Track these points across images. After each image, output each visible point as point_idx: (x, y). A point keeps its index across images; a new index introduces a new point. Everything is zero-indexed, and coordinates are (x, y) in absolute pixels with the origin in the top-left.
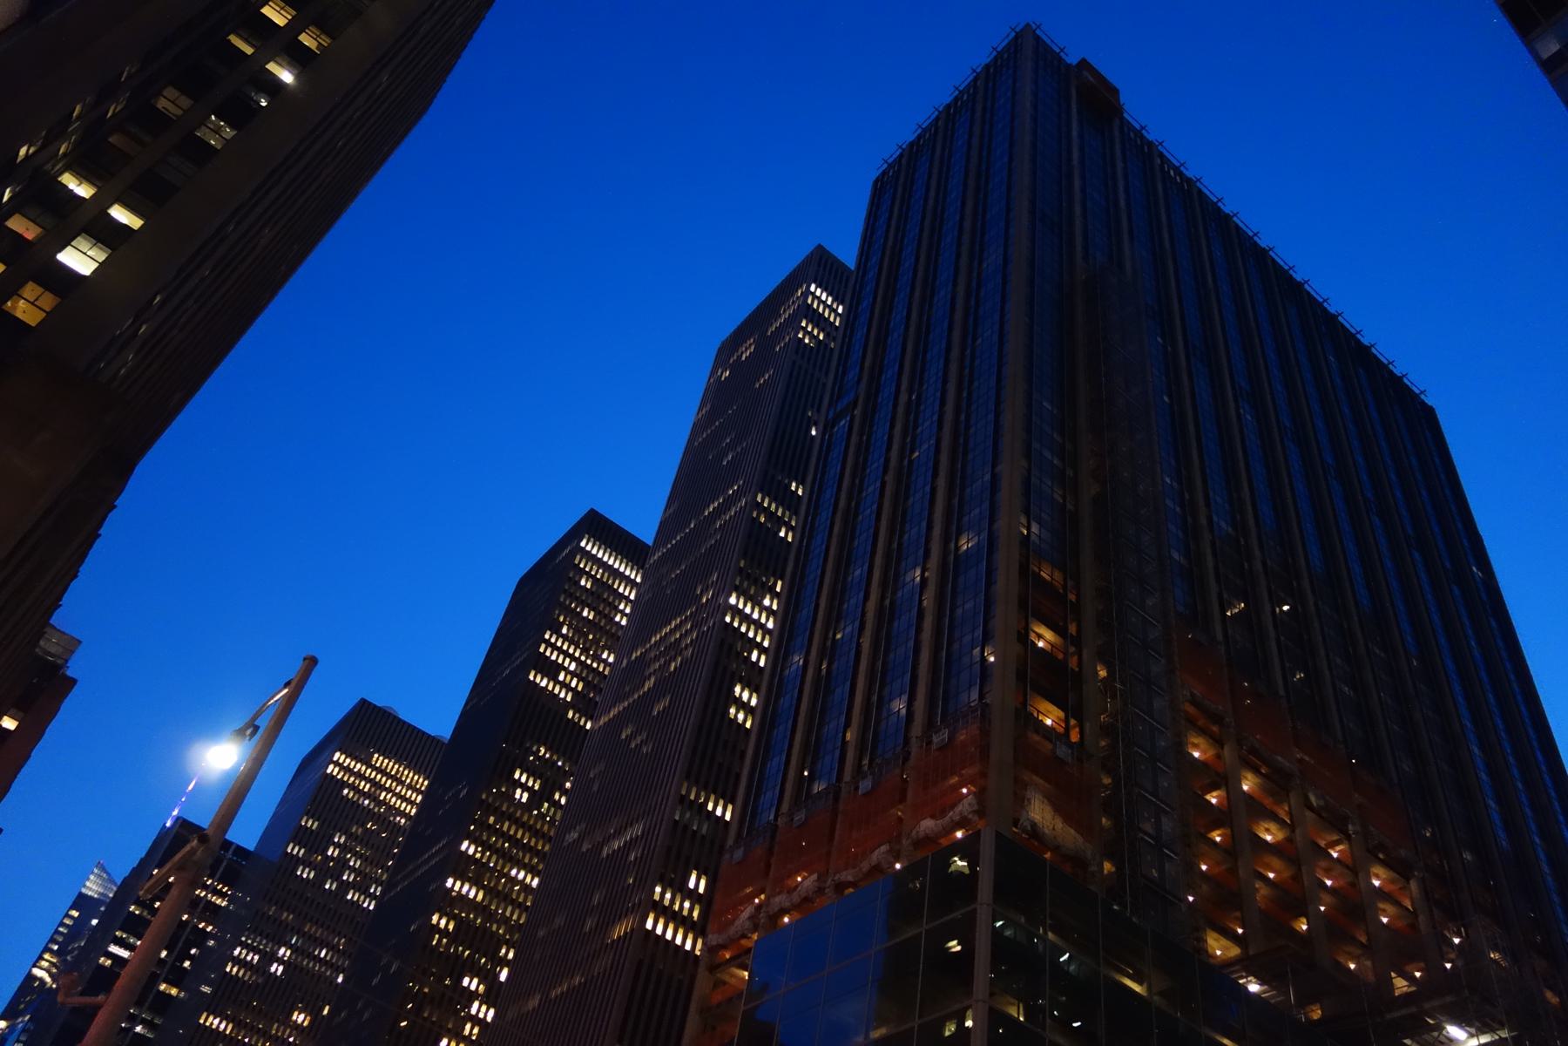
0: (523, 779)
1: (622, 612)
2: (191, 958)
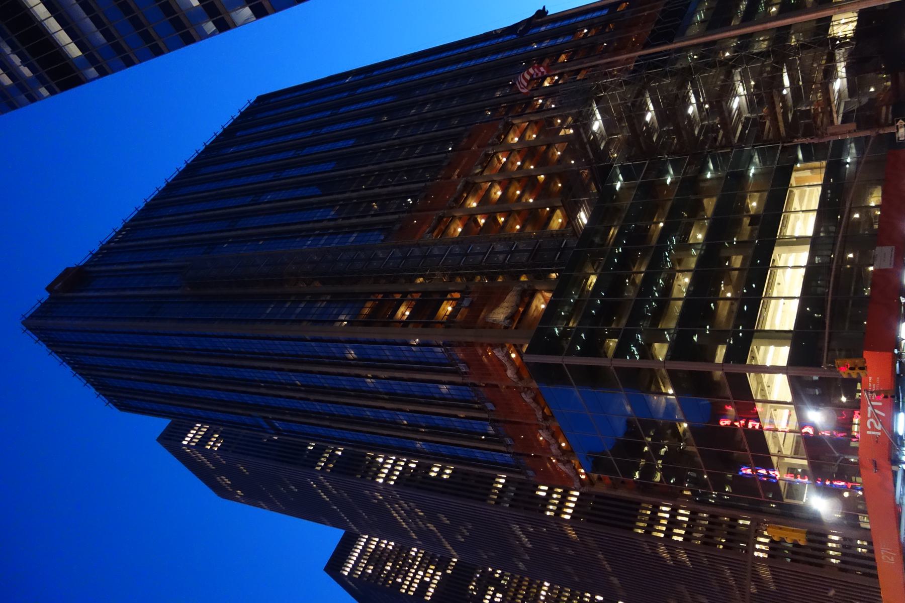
1: (386, 545)
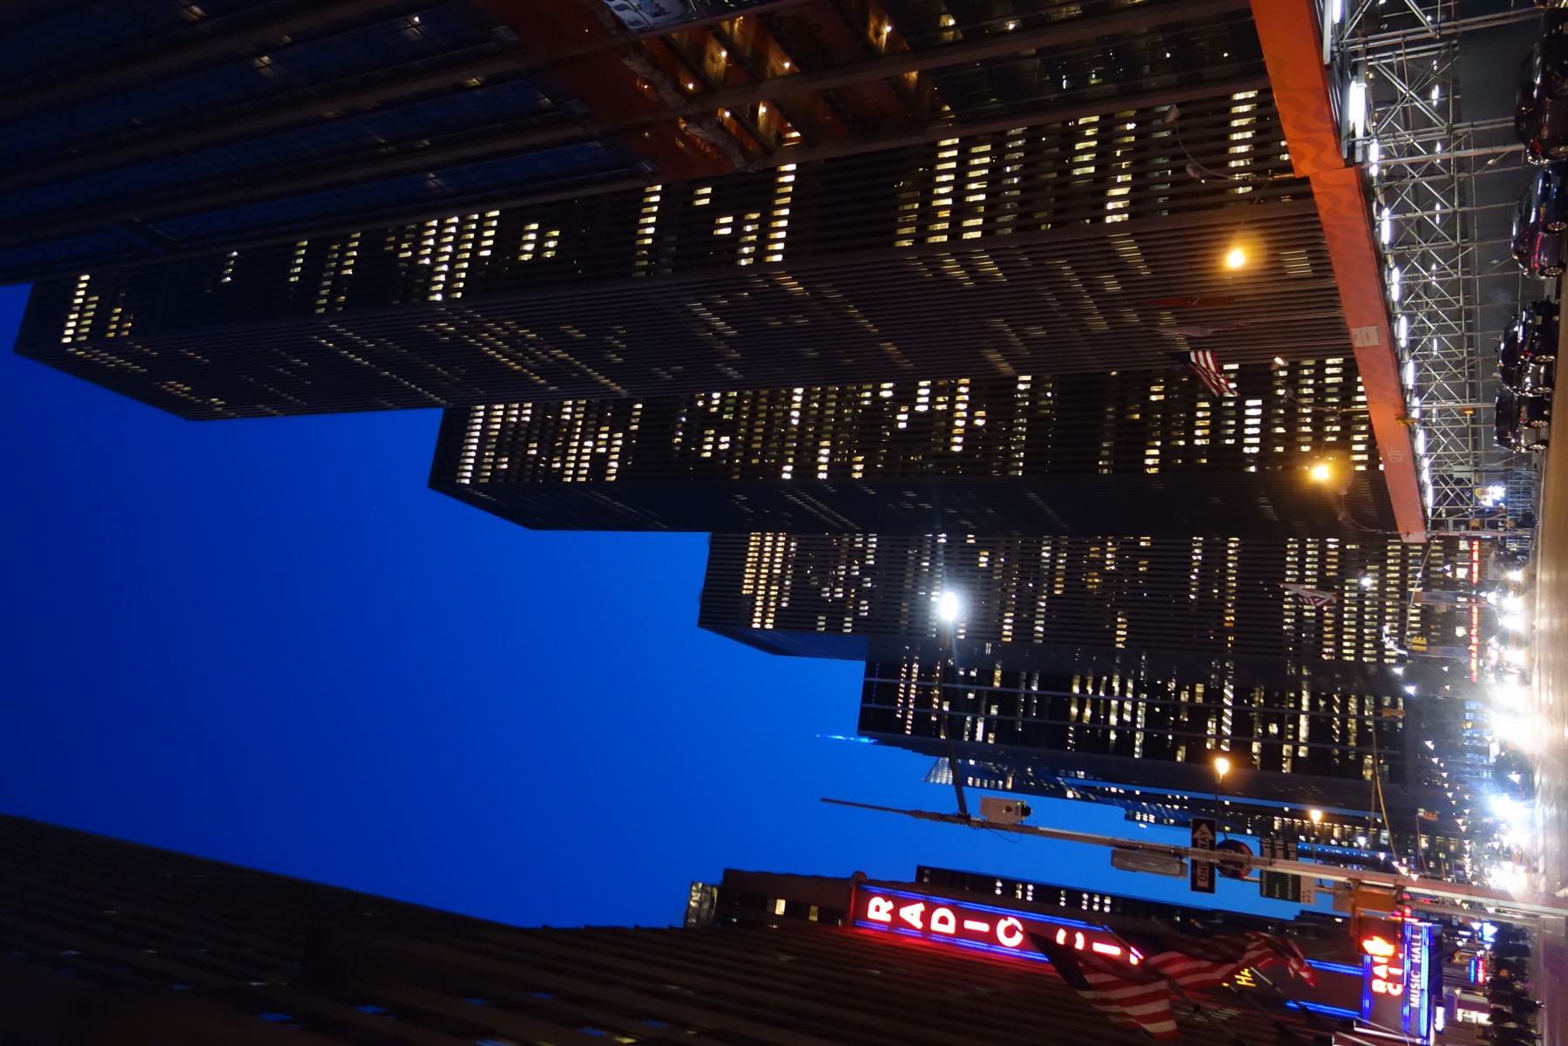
0: (709, 447)
2: (967, 672)
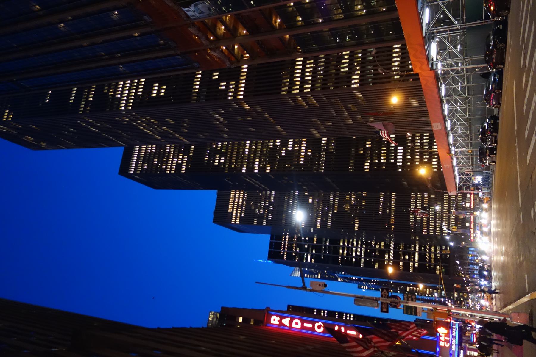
0: (217, 161)
